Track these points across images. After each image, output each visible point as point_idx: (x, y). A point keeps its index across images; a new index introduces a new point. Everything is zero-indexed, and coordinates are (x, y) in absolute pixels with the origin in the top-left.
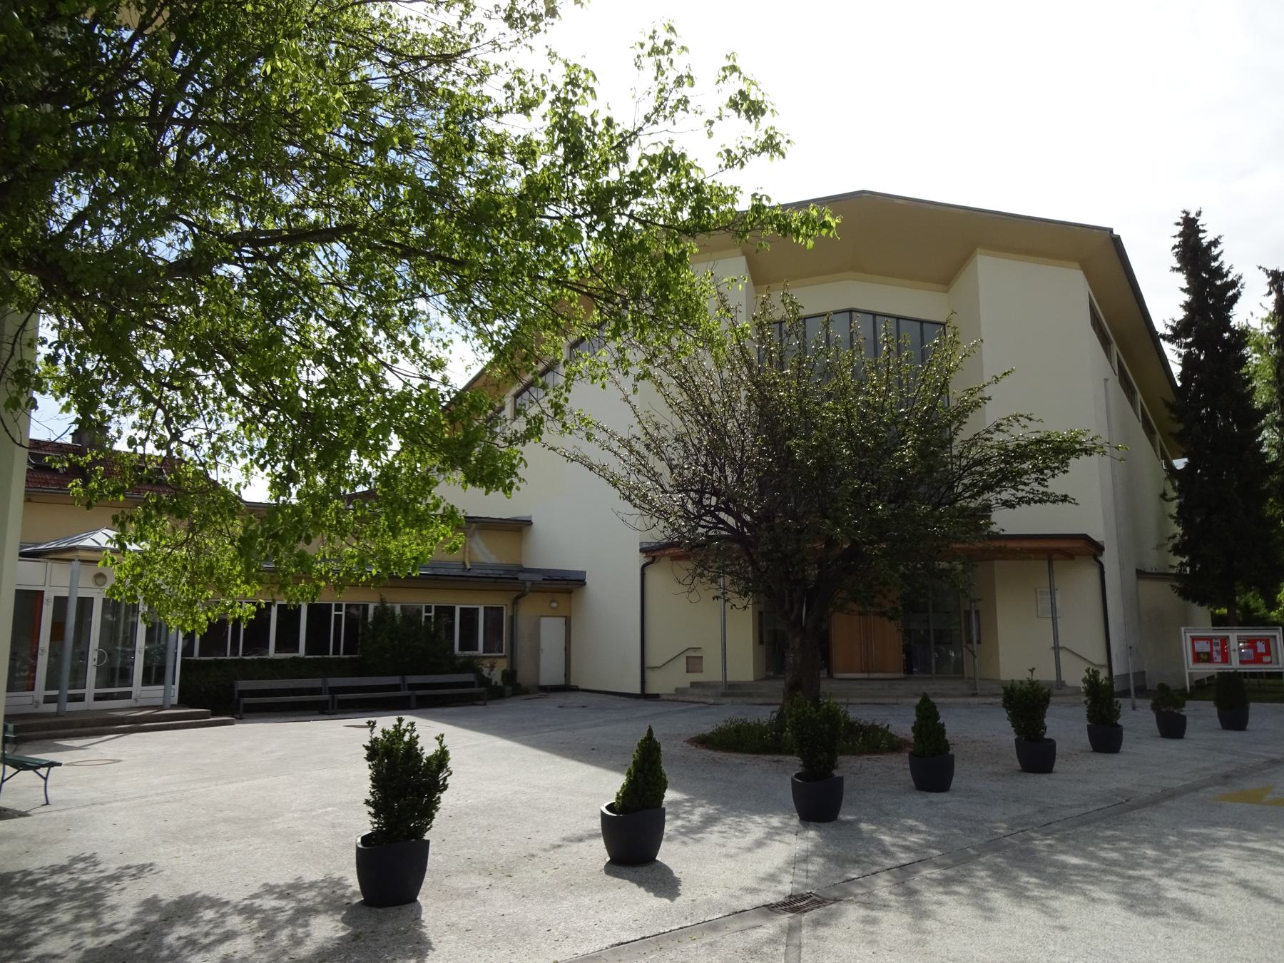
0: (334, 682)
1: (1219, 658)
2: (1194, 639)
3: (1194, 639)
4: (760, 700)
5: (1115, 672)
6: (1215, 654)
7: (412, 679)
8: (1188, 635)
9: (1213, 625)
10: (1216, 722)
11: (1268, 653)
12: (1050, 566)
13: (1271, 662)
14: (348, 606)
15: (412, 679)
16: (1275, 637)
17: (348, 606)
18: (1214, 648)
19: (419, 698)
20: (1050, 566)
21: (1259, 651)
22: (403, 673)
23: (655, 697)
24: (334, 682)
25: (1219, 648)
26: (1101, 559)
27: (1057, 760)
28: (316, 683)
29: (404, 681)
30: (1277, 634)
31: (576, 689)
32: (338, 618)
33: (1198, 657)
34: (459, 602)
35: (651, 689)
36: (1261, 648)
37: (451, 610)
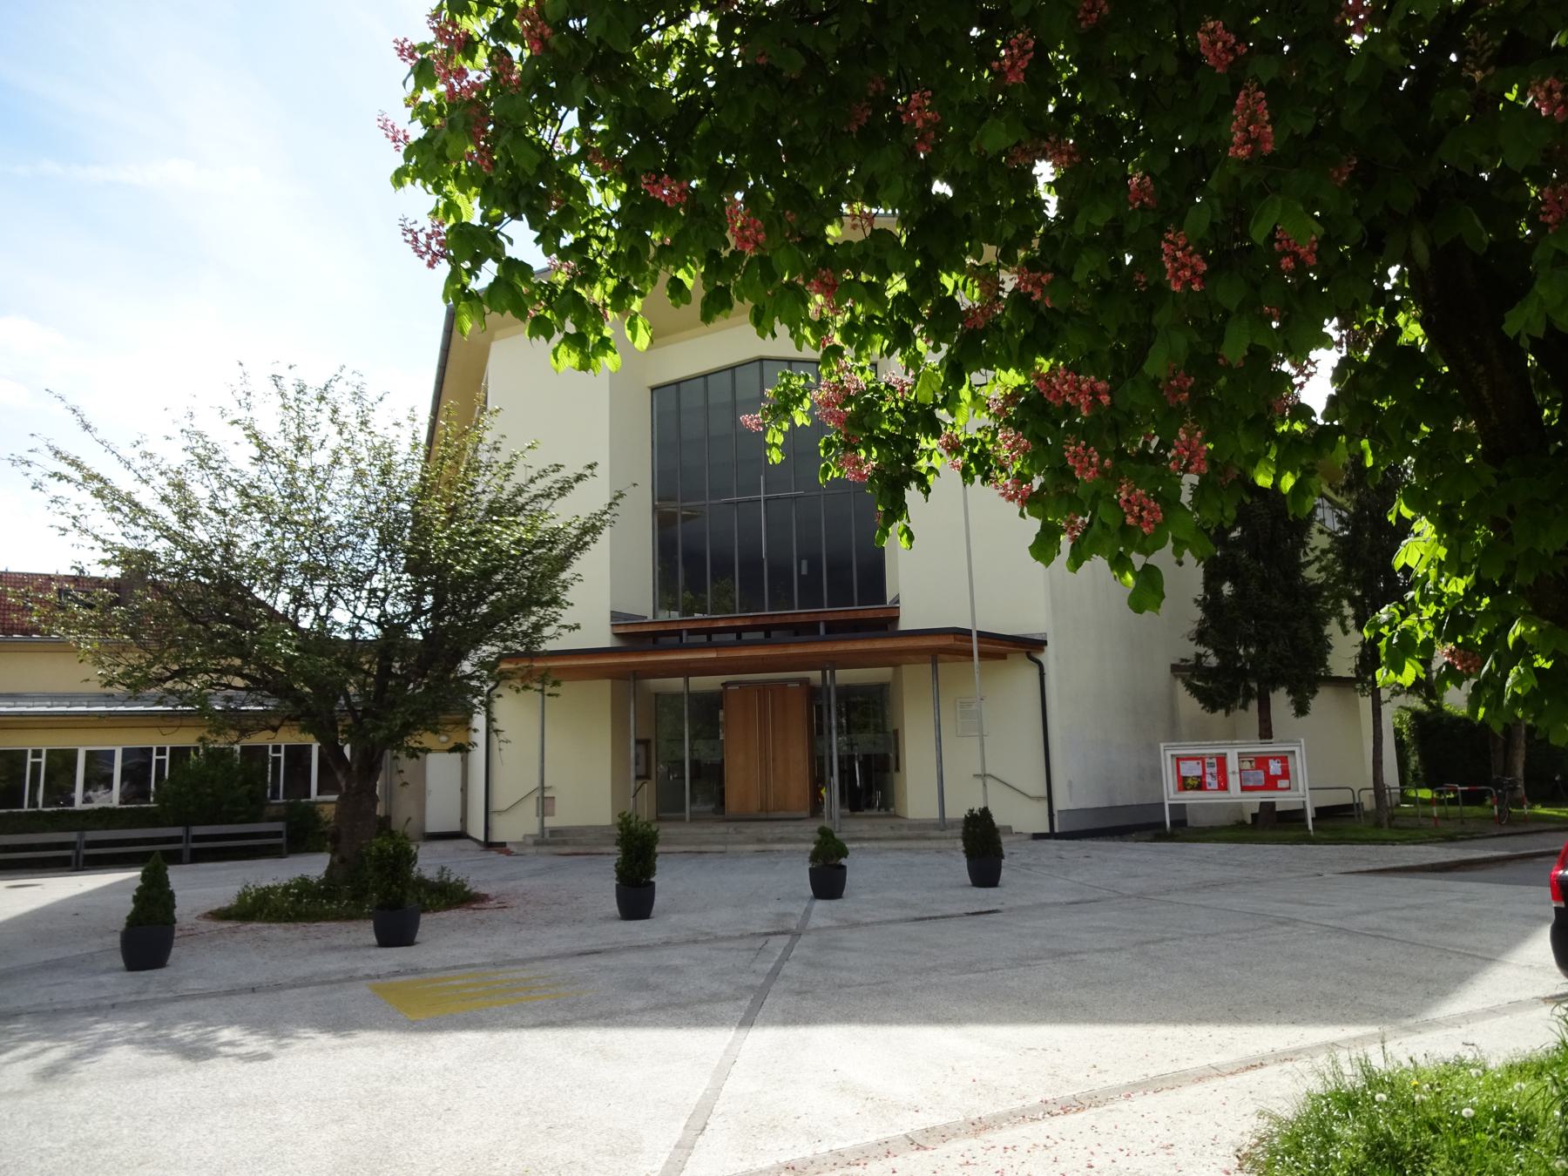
0: (91, 835)
1: (1215, 785)
2: (1179, 759)
3: (1179, 759)
4: (567, 850)
5: (1059, 805)
6: (1208, 779)
7: (198, 830)
8: (1169, 753)
9: (1261, 738)
10: (965, 877)
11: (1285, 774)
12: (935, 672)
13: (1289, 788)
14: (49, 752)
15: (198, 830)
16: (1293, 752)
17: (172, 749)
18: (1208, 770)
19: (194, 851)
20: (935, 672)
21: (1272, 773)
22: (186, 822)
23: (501, 847)
24: (91, 835)
25: (1215, 770)
26: (1041, 657)
27: (118, 945)
28: (72, 837)
29: (187, 831)
30: (1297, 750)
31: (469, 837)
32: (36, 766)
33: (1184, 784)
34: (82, 745)
35: (497, 837)
36: (1275, 768)
37: (70, 756)
